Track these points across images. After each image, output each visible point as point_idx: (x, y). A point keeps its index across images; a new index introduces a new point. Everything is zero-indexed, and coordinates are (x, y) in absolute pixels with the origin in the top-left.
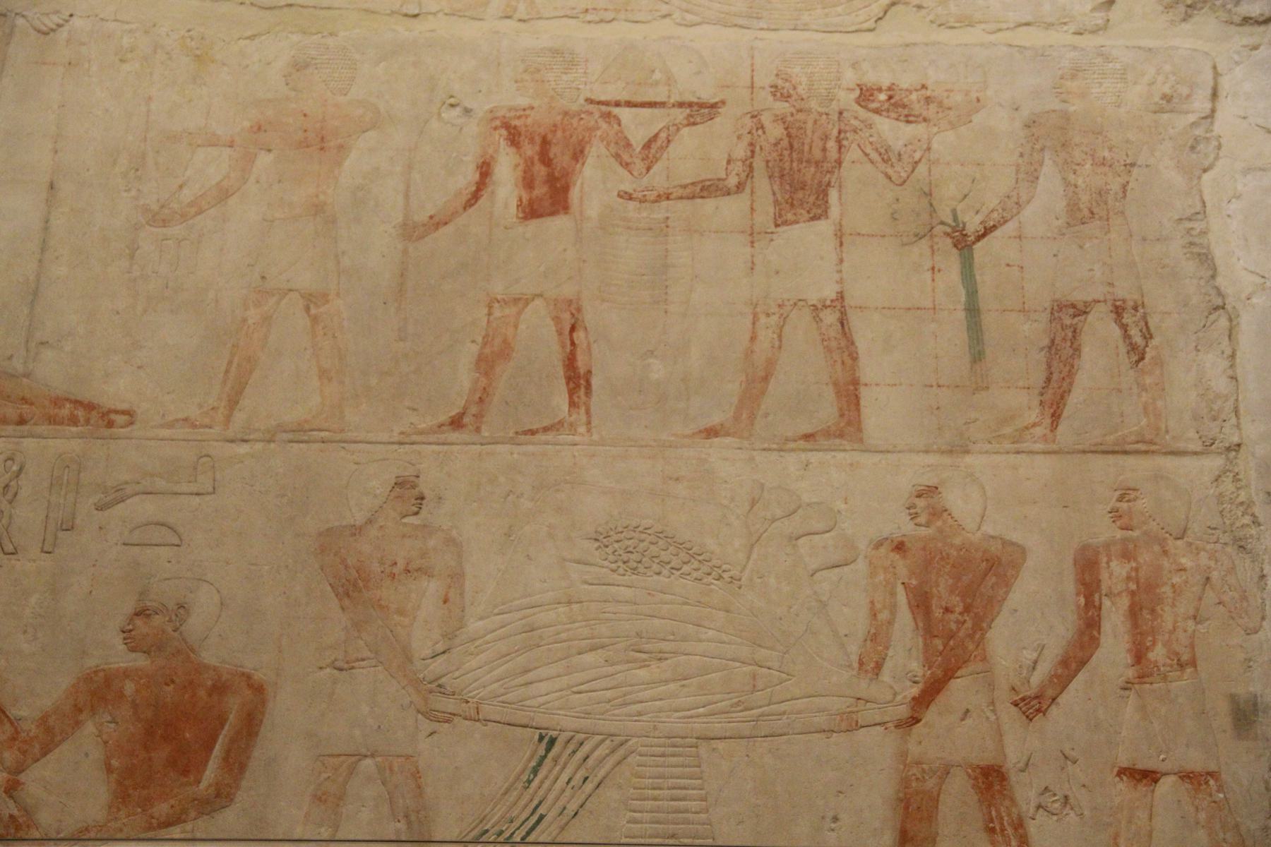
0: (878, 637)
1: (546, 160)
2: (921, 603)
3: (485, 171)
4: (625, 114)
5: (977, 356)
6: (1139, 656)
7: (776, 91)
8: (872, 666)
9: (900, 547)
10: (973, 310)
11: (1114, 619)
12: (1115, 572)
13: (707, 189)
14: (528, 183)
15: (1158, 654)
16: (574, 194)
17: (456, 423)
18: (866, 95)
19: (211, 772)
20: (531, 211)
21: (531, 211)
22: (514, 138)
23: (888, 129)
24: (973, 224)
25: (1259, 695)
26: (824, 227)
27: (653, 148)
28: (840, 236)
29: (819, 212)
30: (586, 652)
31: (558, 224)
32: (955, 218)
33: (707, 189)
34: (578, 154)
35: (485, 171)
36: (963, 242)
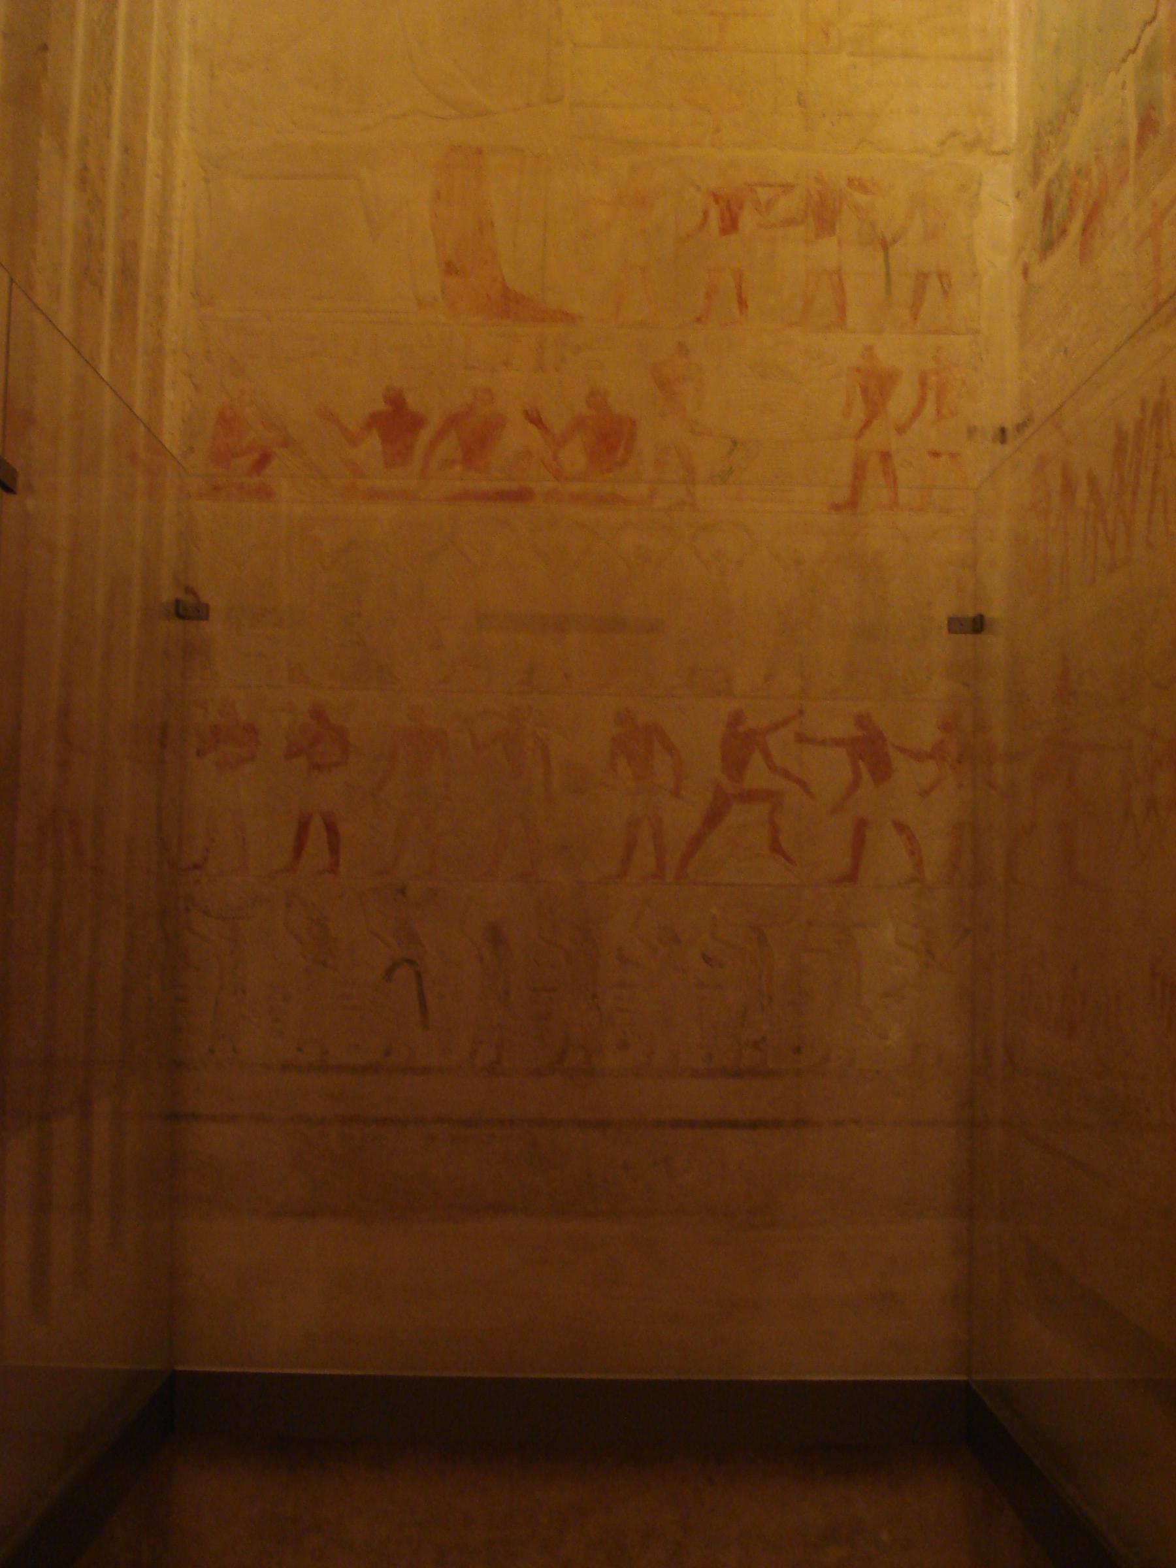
0: (849, 405)
1: (729, 209)
2: (865, 391)
3: (706, 214)
4: (759, 189)
5: (888, 291)
6: (938, 411)
7: (816, 179)
8: (847, 414)
9: (858, 370)
10: (888, 274)
11: (931, 397)
12: (933, 380)
13: (790, 222)
14: (722, 219)
15: (945, 411)
16: (740, 225)
17: (699, 320)
18: (850, 181)
19: (621, 452)
20: (724, 231)
21: (724, 231)
22: (717, 201)
23: (861, 198)
24: (889, 237)
25: (181, 595)
26: (834, 239)
27: (770, 204)
28: (840, 242)
29: (831, 231)
30: (896, 494)
31: (734, 237)
32: (883, 236)
33: (790, 222)
34: (741, 208)
35: (706, 214)
36: (885, 246)
